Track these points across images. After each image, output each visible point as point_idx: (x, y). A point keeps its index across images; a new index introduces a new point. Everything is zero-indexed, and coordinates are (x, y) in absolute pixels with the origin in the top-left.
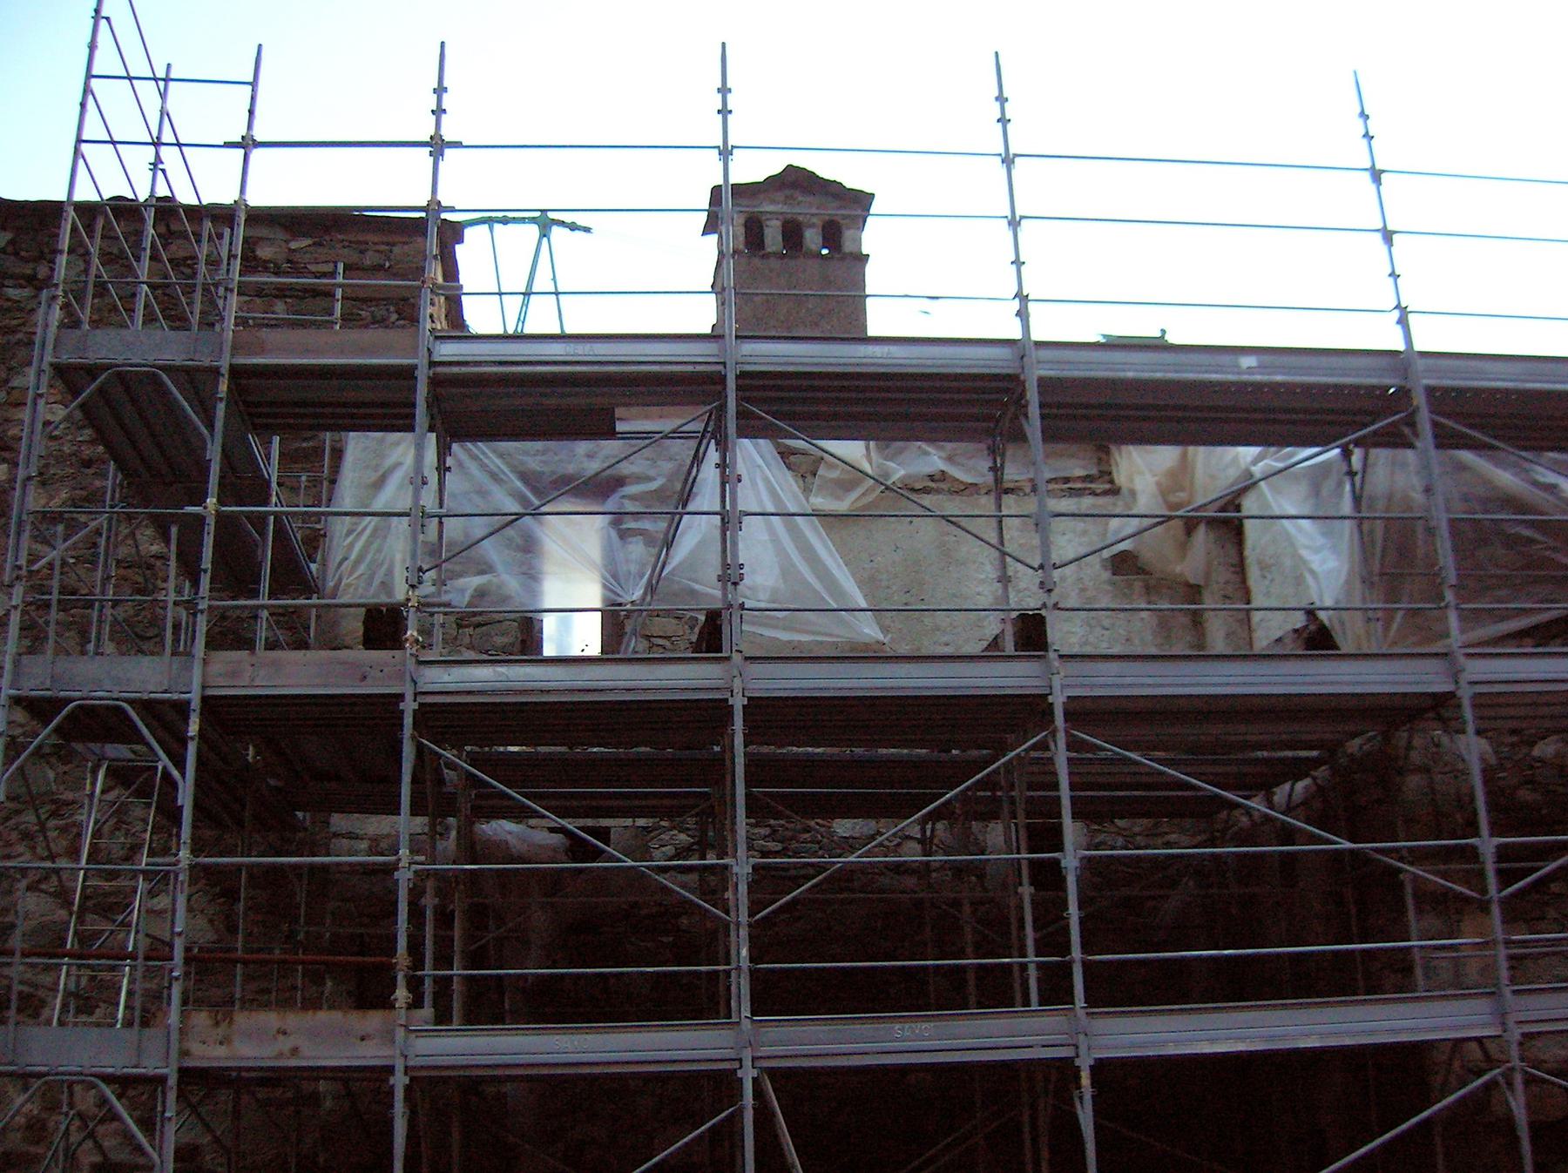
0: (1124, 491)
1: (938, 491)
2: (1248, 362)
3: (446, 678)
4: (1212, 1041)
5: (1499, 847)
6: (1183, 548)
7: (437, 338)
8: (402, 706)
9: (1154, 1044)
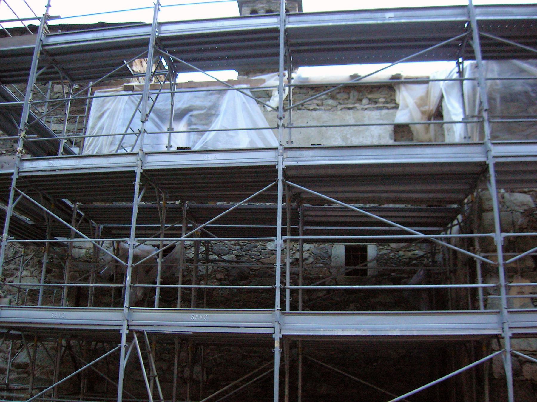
1: (320, 110)
2: (388, 15)
3: (31, 166)
4: (343, 329)
5: (506, 238)
6: (427, 130)
7: (47, 36)
8: (12, 177)
9: (314, 329)
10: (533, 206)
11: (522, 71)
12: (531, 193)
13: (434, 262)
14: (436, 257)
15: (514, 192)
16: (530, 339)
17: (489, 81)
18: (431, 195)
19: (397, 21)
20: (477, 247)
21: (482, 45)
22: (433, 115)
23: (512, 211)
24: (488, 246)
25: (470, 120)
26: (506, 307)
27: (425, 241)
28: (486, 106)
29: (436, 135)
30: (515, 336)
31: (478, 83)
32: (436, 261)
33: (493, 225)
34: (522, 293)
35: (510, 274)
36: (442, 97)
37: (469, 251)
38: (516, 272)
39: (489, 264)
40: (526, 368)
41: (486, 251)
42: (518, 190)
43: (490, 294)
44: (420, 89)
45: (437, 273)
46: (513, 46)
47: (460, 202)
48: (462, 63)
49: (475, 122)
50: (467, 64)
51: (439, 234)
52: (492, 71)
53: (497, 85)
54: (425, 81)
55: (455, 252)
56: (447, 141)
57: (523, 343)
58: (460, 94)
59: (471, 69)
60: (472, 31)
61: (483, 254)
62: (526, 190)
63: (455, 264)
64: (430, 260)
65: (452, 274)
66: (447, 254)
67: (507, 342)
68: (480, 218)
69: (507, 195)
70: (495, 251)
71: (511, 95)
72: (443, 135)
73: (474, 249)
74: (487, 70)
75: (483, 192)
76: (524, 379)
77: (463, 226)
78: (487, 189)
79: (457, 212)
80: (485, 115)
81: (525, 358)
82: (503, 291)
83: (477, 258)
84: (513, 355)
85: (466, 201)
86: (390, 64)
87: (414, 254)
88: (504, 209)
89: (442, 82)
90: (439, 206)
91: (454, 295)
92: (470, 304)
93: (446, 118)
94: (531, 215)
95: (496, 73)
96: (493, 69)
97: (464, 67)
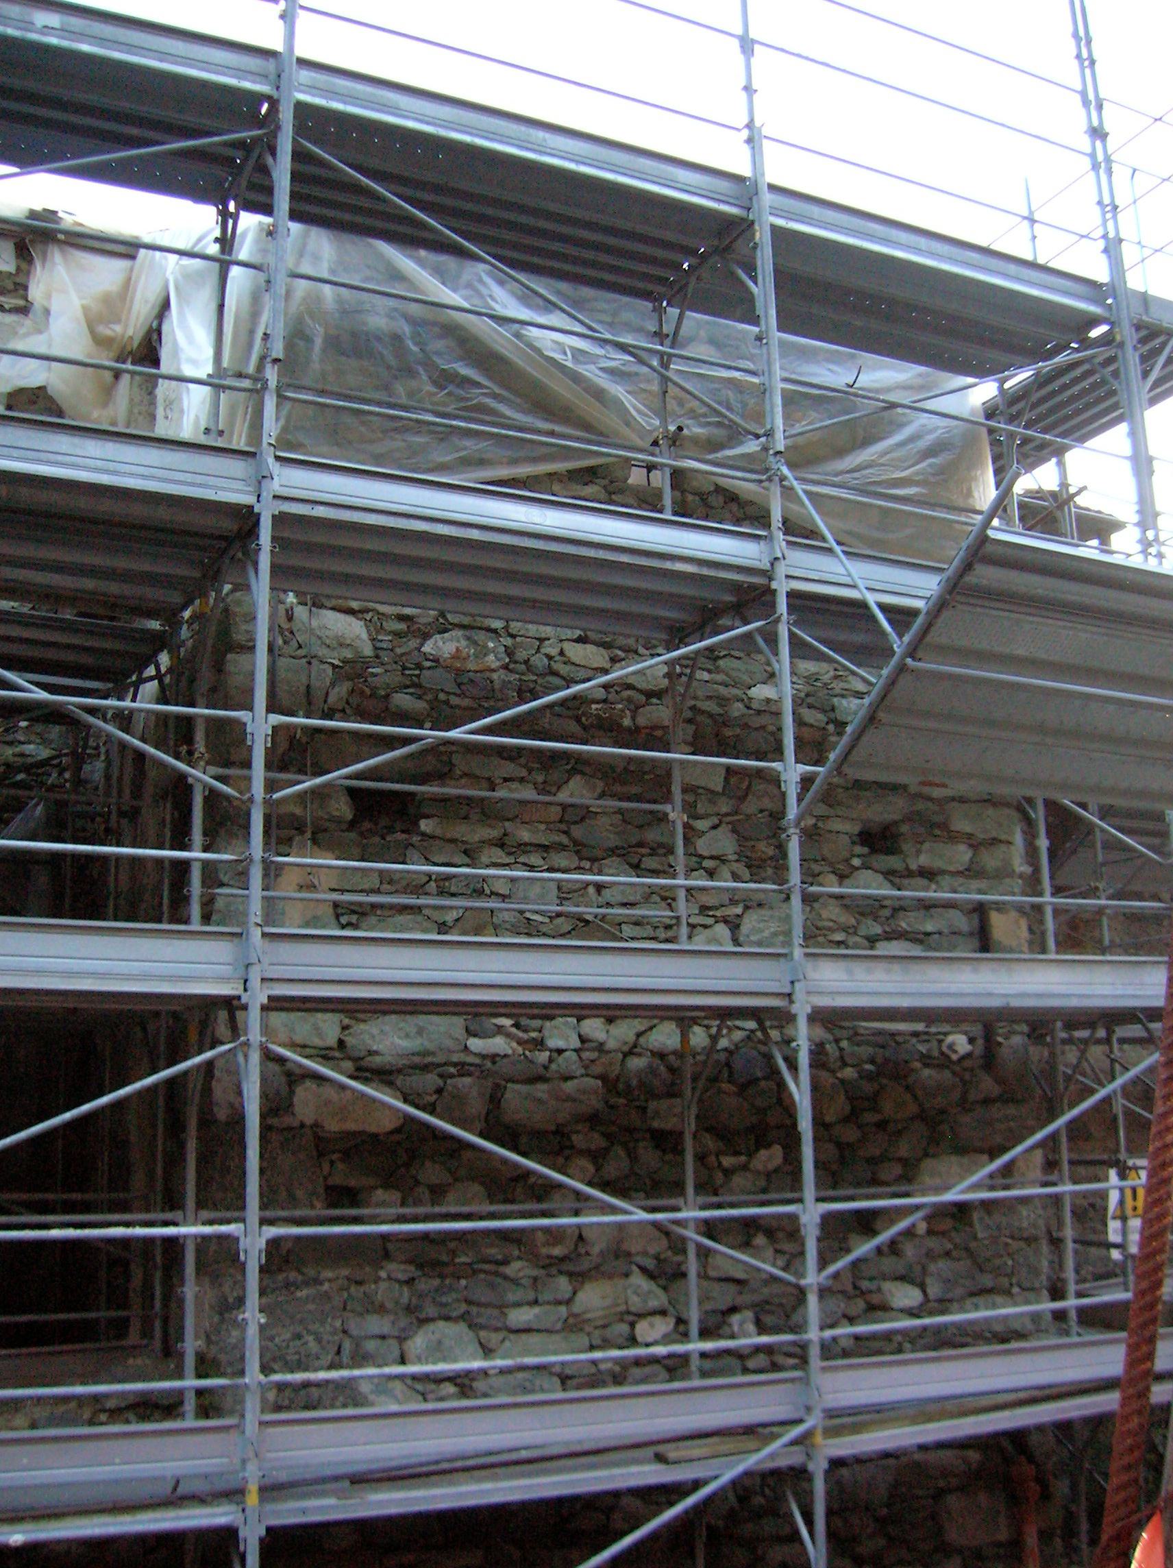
0: (37, 306)
6: (107, 393)
10: (368, 651)
11: (398, 276)
12: (368, 616)
13: (79, 782)
14: (87, 768)
15: (322, 606)
16: (319, 1015)
17: (303, 283)
18: (89, 584)
19: (65, 44)
20: (200, 746)
21: (295, 176)
22: (130, 353)
23: (310, 659)
24: (228, 747)
25: (228, 382)
26: (259, 921)
27: (54, 715)
28: (278, 350)
29: (130, 412)
30: (276, 1004)
31: (269, 282)
32: (86, 782)
33: (250, 692)
34: (312, 887)
35: (284, 833)
36: (166, 305)
37: (177, 757)
38: (300, 830)
39: (228, 798)
40: (304, 1095)
41: (228, 764)
42: (334, 602)
43: (222, 885)
44: (104, 273)
45: (80, 815)
46: (385, 200)
47: (171, 616)
48: (236, 217)
49: (244, 390)
50: (249, 222)
51: (106, 698)
52: (316, 258)
53: (319, 299)
54: (128, 249)
55: (140, 756)
56: (161, 430)
57: (304, 1026)
58: (213, 306)
59: (257, 241)
60: (278, 128)
61: (213, 770)
62: (355, 605)
63: (137, 792)
64: (67, 775)
65: (124, 822)
66: (116, 763)
67: (253, 1020)
68: (219, 667)
69: (301, 612)
70: (248, 764)
71: (354, 335)
72: (153, 417)
73: (190, 753)
74: (301, 254)
75: (238, 594)
76: (296, 1124)
77: (170, 685)
78: (247, 587)
79: (159, 642)
80: (272, 375)
81: (300, 1066)
82: (256, 874)
83: (199, 780)
84: (268, 1056)
85: (187, 614)
86: (15, 170)
87: (22, 755)
88: (289, 650)
89: (173, 258)
90: (112, 619)
91: (124, 885)
92: (165, 908)
93: (165, 367)
94: (360, 676)
95: (325, 265)
96: (320, 250)
97: (239, 231)
